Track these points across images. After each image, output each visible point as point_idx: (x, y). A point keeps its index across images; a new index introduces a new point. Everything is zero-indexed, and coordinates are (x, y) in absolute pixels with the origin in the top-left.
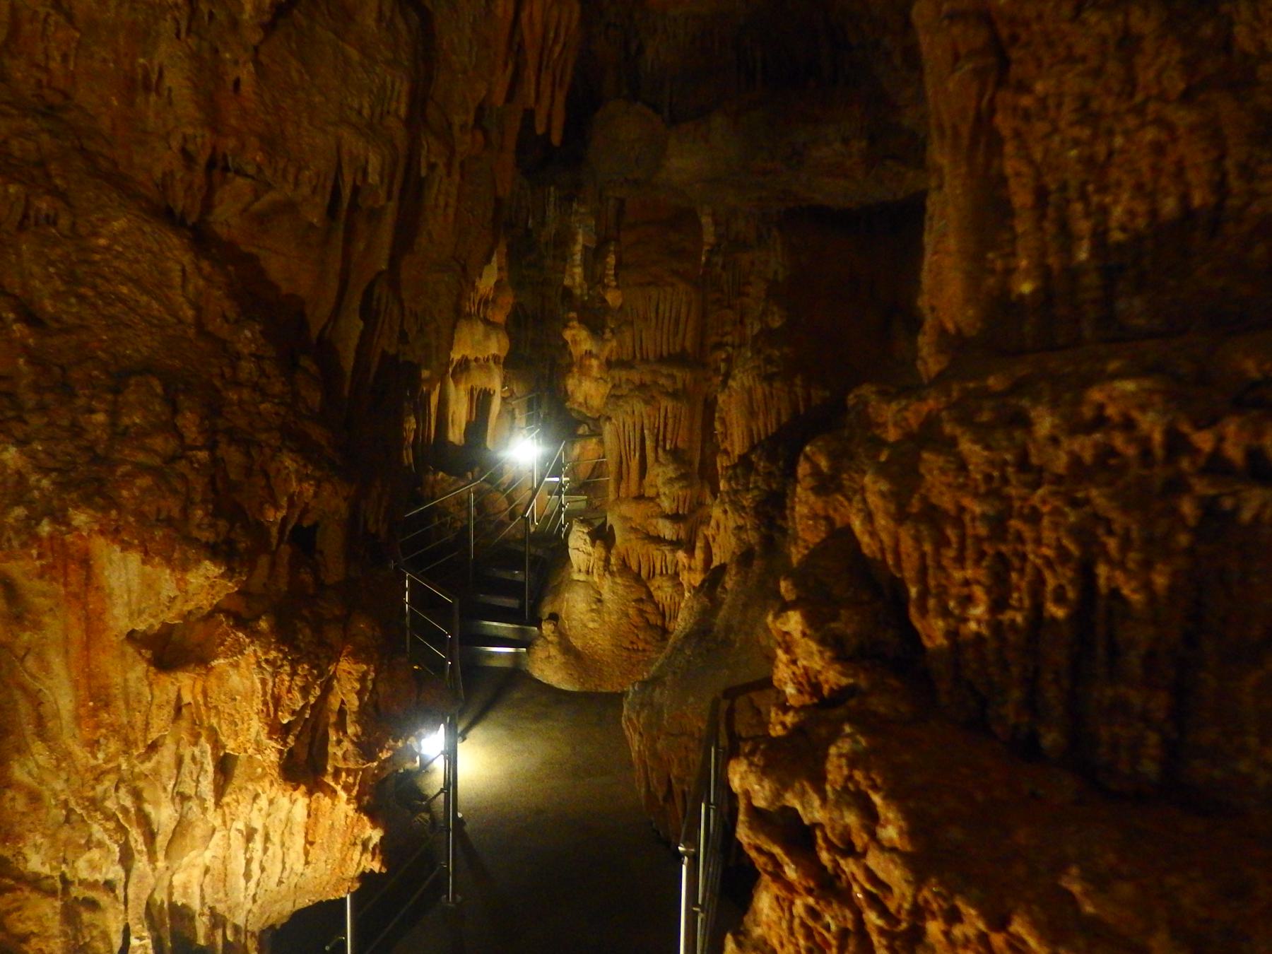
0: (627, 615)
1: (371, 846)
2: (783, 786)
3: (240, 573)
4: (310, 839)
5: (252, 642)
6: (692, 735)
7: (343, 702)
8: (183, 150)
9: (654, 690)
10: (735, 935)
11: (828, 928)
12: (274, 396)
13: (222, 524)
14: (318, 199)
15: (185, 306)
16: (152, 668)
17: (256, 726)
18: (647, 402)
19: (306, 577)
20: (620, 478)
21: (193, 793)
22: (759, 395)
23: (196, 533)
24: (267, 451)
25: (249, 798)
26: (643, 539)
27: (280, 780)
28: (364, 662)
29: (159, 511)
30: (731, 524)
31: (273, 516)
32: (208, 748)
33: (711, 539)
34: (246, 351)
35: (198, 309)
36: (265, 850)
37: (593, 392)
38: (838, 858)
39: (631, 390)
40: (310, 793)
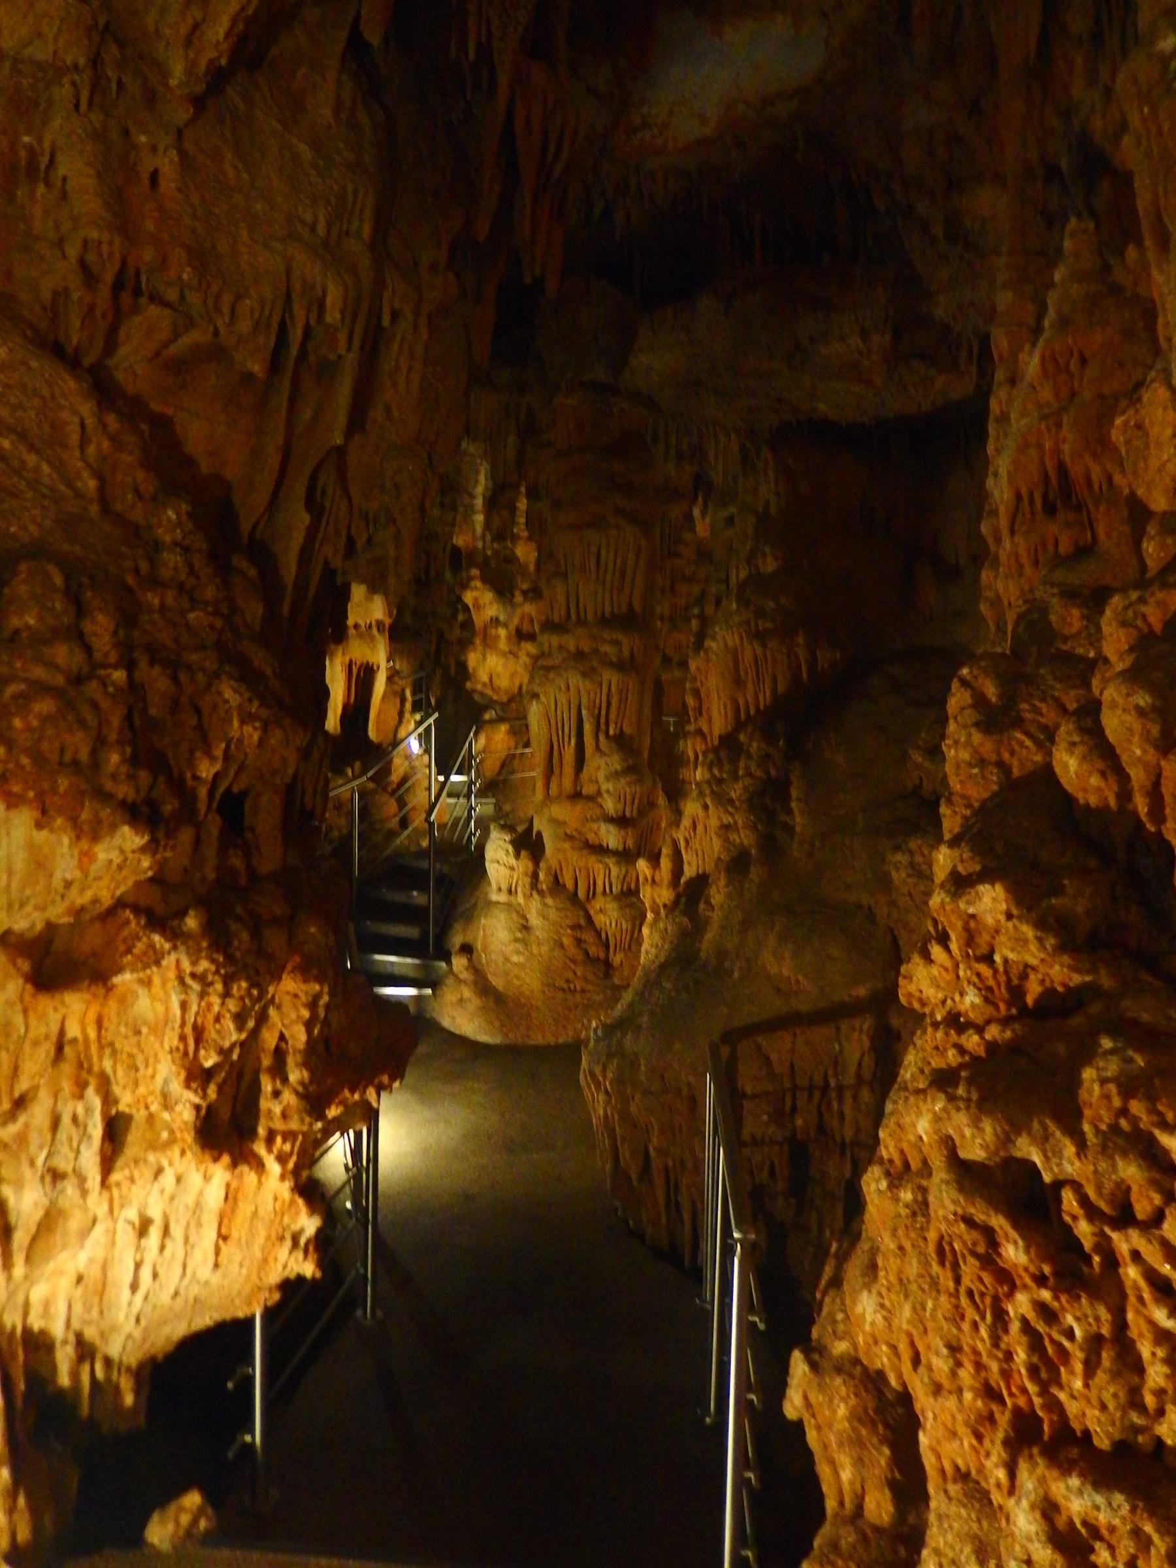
0: (562, 946)
1: (303, 1241)
2: (1014, 1127)
3: (165, 848)
4: (224, 1231)
5: (175, 948)
6: (678, 1091)
7: (282, 1037)
8: (83, 265)
9: (624, 1035)
10: (807, 1353)
11: (1070, 1334)
12: (206, 603)
13: (144, 776)
14: (261, 340)
15: (86, 474)
16: (29, 987)
17: (166, 1072)
18: (585, 675)
19: (237, 862)
20: (549, 773)
21: (70, 1169)
22: (748, 657)
23: (109, 785)
24: (200, 676)
25: (148, 1173)
26: (581, 849)
27: (196, 1148)
28: (319, 980)
29: (62, 750)
30: (714, 823)
31: (206, 770)
32: (97, 1103)
33: (682, 844)
34: (168, 538)
35: (101, 478)
36: (162, 1248)
37: (500, 669)
38: (1107, 1230)
39: (564, 660)
40: (234, 1164)
